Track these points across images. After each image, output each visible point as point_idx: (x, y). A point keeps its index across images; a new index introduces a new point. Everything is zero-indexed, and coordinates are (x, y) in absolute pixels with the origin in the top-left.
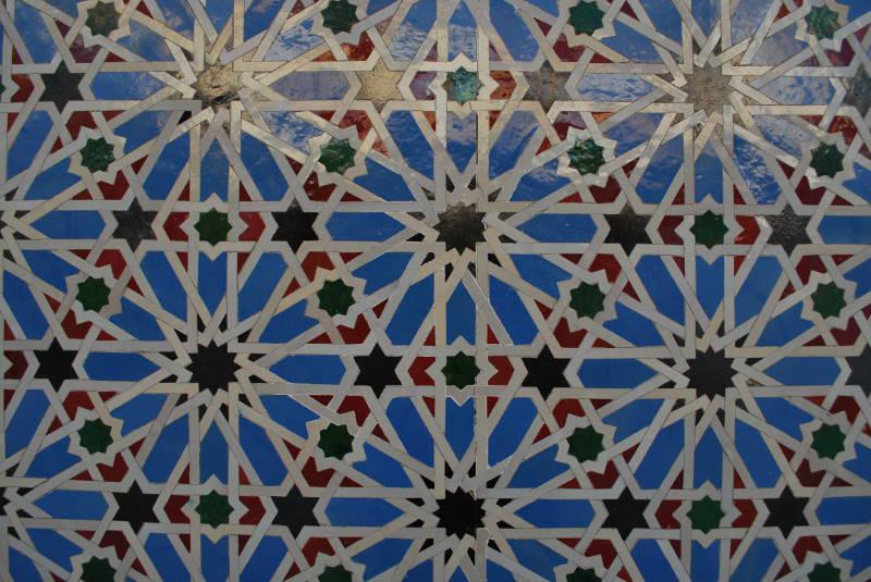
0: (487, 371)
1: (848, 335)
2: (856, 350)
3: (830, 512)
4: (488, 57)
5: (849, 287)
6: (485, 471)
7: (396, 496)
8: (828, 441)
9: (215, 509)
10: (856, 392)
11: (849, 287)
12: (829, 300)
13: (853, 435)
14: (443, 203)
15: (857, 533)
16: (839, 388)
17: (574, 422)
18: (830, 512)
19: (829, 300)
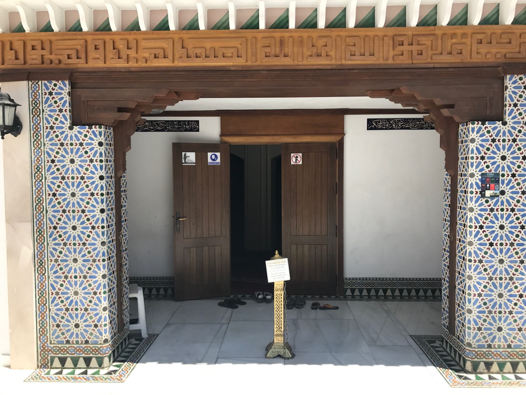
0: (84, 138)
1: (523, 83)
2: (524, 85)
3: (521, 105)
4: (13, 136)
5: (523, 112)
6: (74, 133)
7: (82, 320)
8: (521, 96)
9: (486, 219)
10: (524, 90)
11: (523, 112)
12: (520, 114)
13: (524, 95)
14: (73, 231)
15: (524, 143)
16: (522, 90)
17: (520, 187)
18: (521, 105)
19: (520, 114)
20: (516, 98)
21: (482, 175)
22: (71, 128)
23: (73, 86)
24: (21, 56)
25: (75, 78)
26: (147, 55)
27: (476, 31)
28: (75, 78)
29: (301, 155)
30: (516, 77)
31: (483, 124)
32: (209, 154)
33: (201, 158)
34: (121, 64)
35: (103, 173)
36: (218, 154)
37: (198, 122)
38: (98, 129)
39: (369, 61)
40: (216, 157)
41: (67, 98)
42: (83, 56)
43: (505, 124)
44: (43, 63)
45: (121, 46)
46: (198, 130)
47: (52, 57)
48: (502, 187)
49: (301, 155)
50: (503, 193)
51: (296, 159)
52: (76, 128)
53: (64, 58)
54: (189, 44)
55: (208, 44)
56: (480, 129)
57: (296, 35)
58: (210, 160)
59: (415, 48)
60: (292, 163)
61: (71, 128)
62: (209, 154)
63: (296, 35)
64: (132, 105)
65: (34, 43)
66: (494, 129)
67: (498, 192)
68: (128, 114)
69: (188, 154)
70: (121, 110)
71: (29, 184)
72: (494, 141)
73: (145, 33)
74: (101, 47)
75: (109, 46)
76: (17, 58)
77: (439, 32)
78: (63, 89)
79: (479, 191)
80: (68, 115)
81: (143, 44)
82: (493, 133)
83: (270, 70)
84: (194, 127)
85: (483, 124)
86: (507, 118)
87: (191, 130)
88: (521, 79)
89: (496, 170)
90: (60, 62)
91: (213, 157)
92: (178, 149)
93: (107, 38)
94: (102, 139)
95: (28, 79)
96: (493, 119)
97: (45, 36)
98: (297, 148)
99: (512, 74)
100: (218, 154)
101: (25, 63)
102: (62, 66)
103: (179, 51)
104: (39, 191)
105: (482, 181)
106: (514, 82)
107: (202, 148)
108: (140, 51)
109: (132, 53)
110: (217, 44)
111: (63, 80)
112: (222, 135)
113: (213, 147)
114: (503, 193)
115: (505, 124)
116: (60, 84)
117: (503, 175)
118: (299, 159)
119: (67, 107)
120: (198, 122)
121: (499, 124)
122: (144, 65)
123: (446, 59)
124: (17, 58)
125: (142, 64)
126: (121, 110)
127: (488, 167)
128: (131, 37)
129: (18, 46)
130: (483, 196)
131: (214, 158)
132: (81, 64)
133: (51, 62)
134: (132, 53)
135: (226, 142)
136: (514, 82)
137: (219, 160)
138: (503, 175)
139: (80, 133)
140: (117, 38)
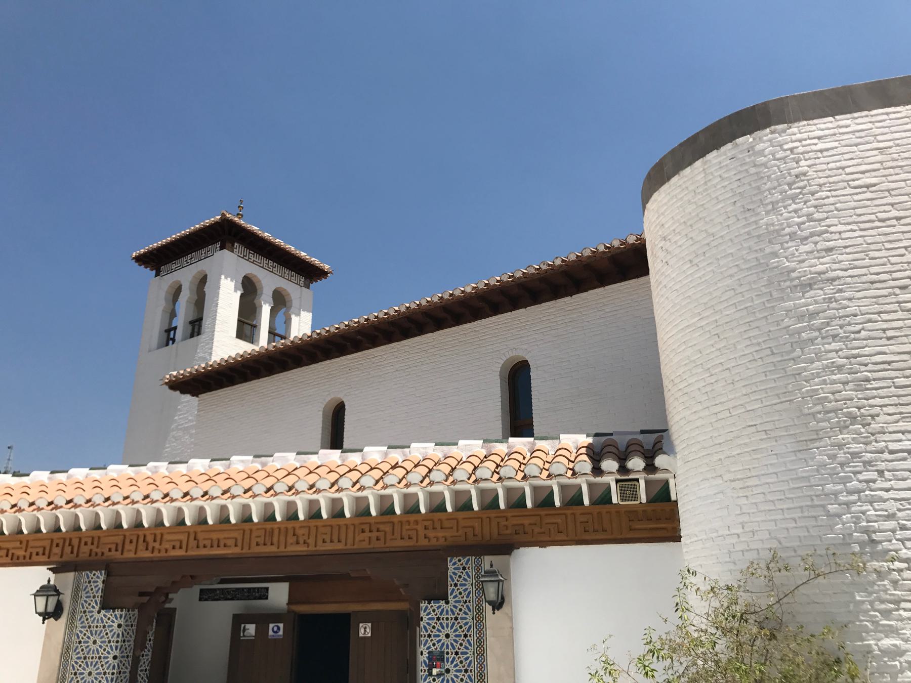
20: (456, 578)
21: (429, 653)
22: (99, 612)
23: (108, 575)
24: (75, 552)
25: (109, 568)
26: (167, 546)
27: (426, 518)
28: (109, 568)
29: (370, 625)
30: (455, 560)
31: (429, 603)
32: (271, 626)
33: (262, 631)
34: (147, 554)
35: (117, 653)
36: (281, 625)
37: (267, 589)
38: (120, 612)
39: (340, 547)
40: (279, 628)
41: (101, 585)
42: (120, 549)
43: (447, 603)
44: (90, 555)
45: (150, 539)
46: (267, 598)
47: (98, 550)
48: (448, 665)
49: (370, 625)
50: (448, 671)
51: (365, 630)
52: (103, 612)
53: (106, 551)
54: (201, 536)
55: (215, 536)
56: (427, 607)
57: (283, 526)
58: (271, 633)
59: (375, 534)
60: (361, 635)
61: (99, 612)
62: (271, 626)
63: (283, 526)
64: (152, 590)
65: (87, 540)
66: (439, 607)
67: (443, 670)
68: (148, 598)
69: (248, 626)
70: (142, 594)
71: (57, 664)
72: (456, 619)
73: (168, 528)
74: (135, 541)
75: (141, 539)
76: (72, 552)
77: (396, 520)
78: (99, 578)
79: (427, 669)
80: (98, 600)
81: (166, 537)
82: (438, 611)
83: (258, 558)
84: (263, 594)
85: (429, 603)
86: (450, 598)
87: (260, 598)
88: (459, 561)
89: (441, 648)
90: (103, 554)
91: (275, 629)
92: (238, 620)
93: (141, 533)
94: (122, 621)
95: (75, 570)
96: (437, 599)
97: (96, 533)
98: (366, 617)
99: (452, 557)
100: (281, 625)
101: (77, 556)
102: (104, 558)
103: (193, 543)
104: (65, 669)
105: (429, 658)
106: (454, 564)
107: (263, 619)
108: (164, 543)
109: (157, 545)
110: (221, 536)
111: (100, 571)
112: (289, 603)
113: (276, 617)
114: (448, 671)
115: (447, 603)
116: (98, 573)
117: (448, 653)
118: (368, 630)
119: (100, 594)
120: (267, 589)
121: (442, 603)
122: (165, 555)
123: (399, 544)
124: (72, 552)
125: (163, 554)
126: (142, 594)
127: (434, 645)
128: (158, 532)
129: (75, 542)
130: (430, 674)
131: (277, 630)
132: (116, 555)
133: (96, 554)
134: (157, 545)
135: (293, 611)
136: (454, 564)
137: (281, 633)
138: (448, 653)
139: (105, 616)
140: (147, 533)
